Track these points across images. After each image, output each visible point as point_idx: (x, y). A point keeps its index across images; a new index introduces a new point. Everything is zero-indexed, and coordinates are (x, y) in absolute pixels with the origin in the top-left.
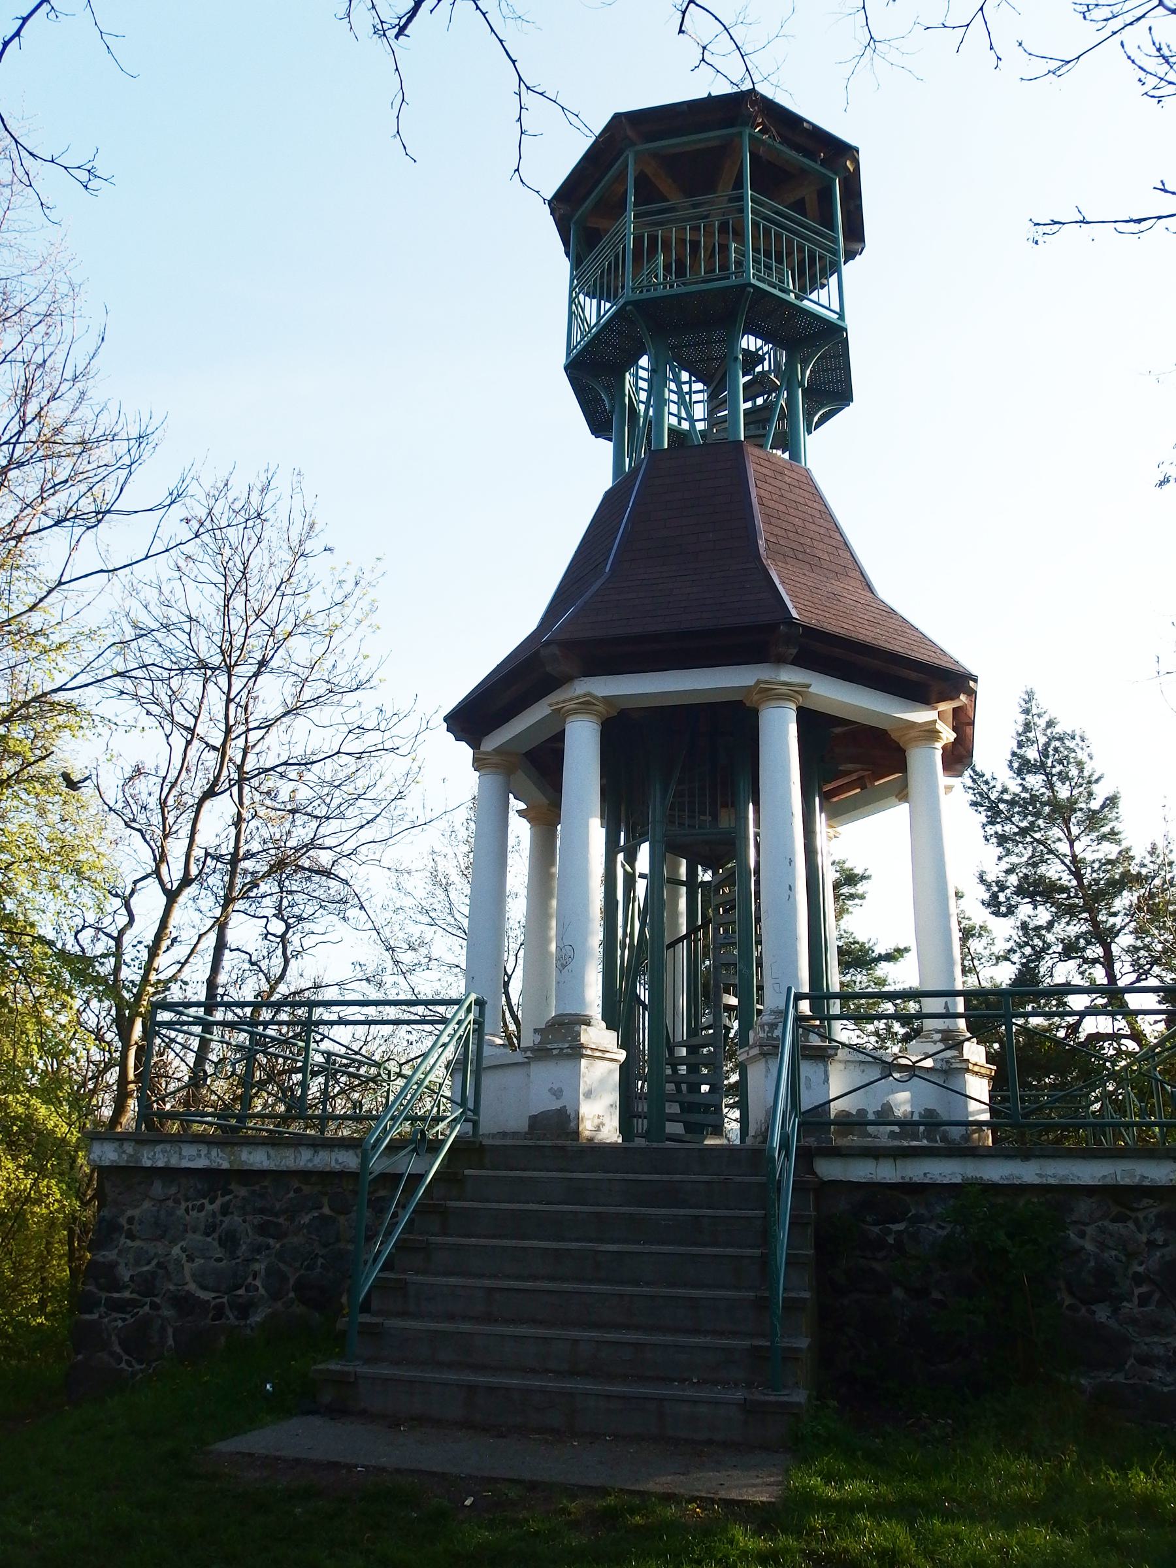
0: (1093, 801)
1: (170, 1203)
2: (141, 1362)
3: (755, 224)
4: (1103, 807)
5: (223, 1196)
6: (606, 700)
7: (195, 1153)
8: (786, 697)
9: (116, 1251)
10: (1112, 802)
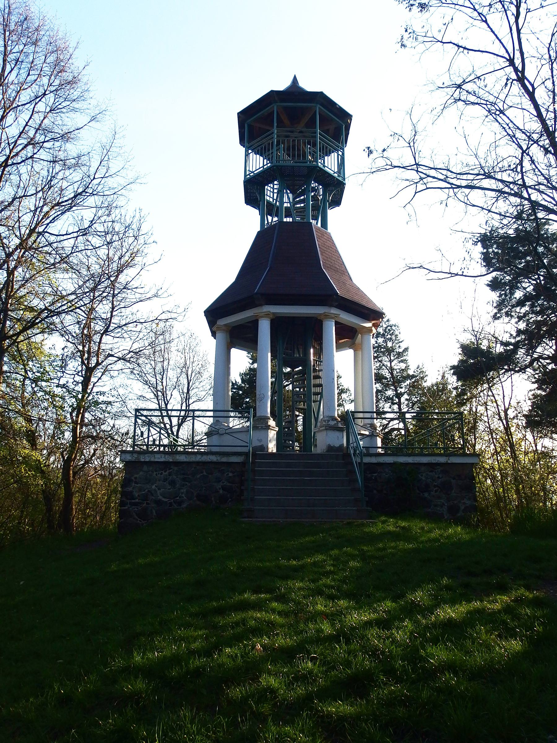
1: (150, 473)
2: (144, 520)
3: (320, 143)
4: (403, 351)
5: (169, 470)
7: (160, 457)
8: (332, 318)
9: (132, 488)
10: (406, 350)
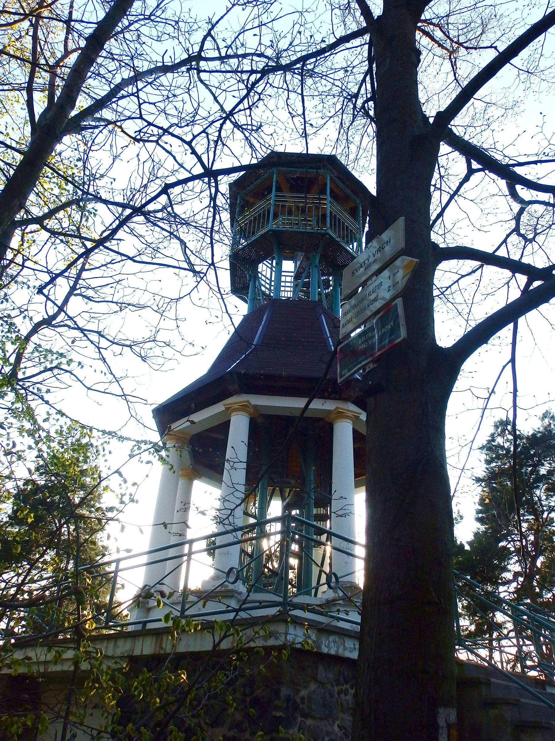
0: (110, 513)
6: (255, 407)
8: (347, 417)
